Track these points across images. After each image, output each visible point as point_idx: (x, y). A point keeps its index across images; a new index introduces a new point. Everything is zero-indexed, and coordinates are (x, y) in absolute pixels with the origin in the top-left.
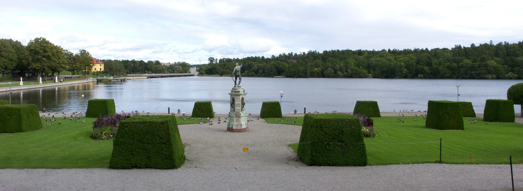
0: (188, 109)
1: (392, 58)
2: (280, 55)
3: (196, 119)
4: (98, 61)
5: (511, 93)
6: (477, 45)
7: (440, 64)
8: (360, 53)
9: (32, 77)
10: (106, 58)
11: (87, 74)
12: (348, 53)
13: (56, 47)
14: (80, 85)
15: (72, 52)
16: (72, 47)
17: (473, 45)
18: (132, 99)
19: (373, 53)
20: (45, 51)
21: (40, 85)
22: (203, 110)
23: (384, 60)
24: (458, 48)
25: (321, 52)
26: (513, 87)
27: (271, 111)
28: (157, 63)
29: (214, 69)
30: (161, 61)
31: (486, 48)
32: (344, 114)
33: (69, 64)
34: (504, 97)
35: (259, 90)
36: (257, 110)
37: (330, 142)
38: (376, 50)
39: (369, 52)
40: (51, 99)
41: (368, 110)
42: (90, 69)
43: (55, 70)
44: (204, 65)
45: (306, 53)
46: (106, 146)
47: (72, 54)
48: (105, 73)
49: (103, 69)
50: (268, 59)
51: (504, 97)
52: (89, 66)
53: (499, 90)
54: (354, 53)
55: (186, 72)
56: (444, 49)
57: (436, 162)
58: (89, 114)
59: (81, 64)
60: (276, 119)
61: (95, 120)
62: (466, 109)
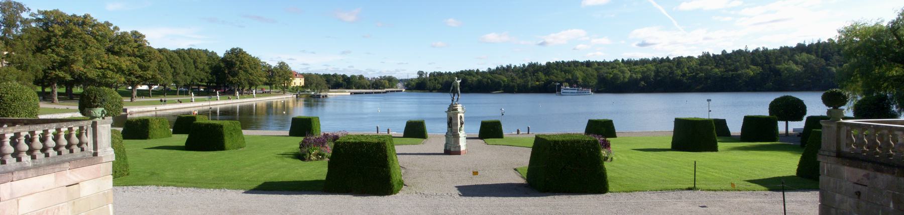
0: (398, 130)
1: (626, 69)
2: (497, 68)
3: (408, 139)
4: (296, 75)
5: (773, 107)
6: (729, 51)
7: (684, 75)
8: (588, 64)
9: (228, 90)
10: (306, 72)
11: (285, 89)
12: (575, 64)
13: (253, 59)
14: (238, 106)
15: (270, 63)
16: (271, 59)
17: (724, 52)
18: (341, 118)
19: (604, 64)
20: (242, 62)
21: (236, 102)
22: (415, 130)
23: (616, 71)
24: (707, 56)
25: (544, 63)
26: (776, 101)
27: (490, 131)
28: (361, 77)
29: (422, 85)
30: (365, 76)
31: (739, 54)
32: (367, 136)
33: (267, 77)
34: (765, 112)
35: (474, 109)
36: (476, 130)
37: (569, 165)
38: (608, 60)
39: (599, 63)
40: (247, 118)
41: (603, 129)
42: (290, 83)
43: (251, 84)
44: (412, 80)
45: (527, 65)
46: (317, 170)
47: (270, 66)
48: (306, 86)
49: (303, 84)
50: (483, 72)
51: (765, 112)
52: (287, 79)
53: (759, 104)
54: (582, 64)
55: (392, 87)
56: (689, 57)
57: (689, 189)
58: (293, 133)
59: (277, 77)
60: (498, 140)
61: (301, 139)
62: (721, 127)
